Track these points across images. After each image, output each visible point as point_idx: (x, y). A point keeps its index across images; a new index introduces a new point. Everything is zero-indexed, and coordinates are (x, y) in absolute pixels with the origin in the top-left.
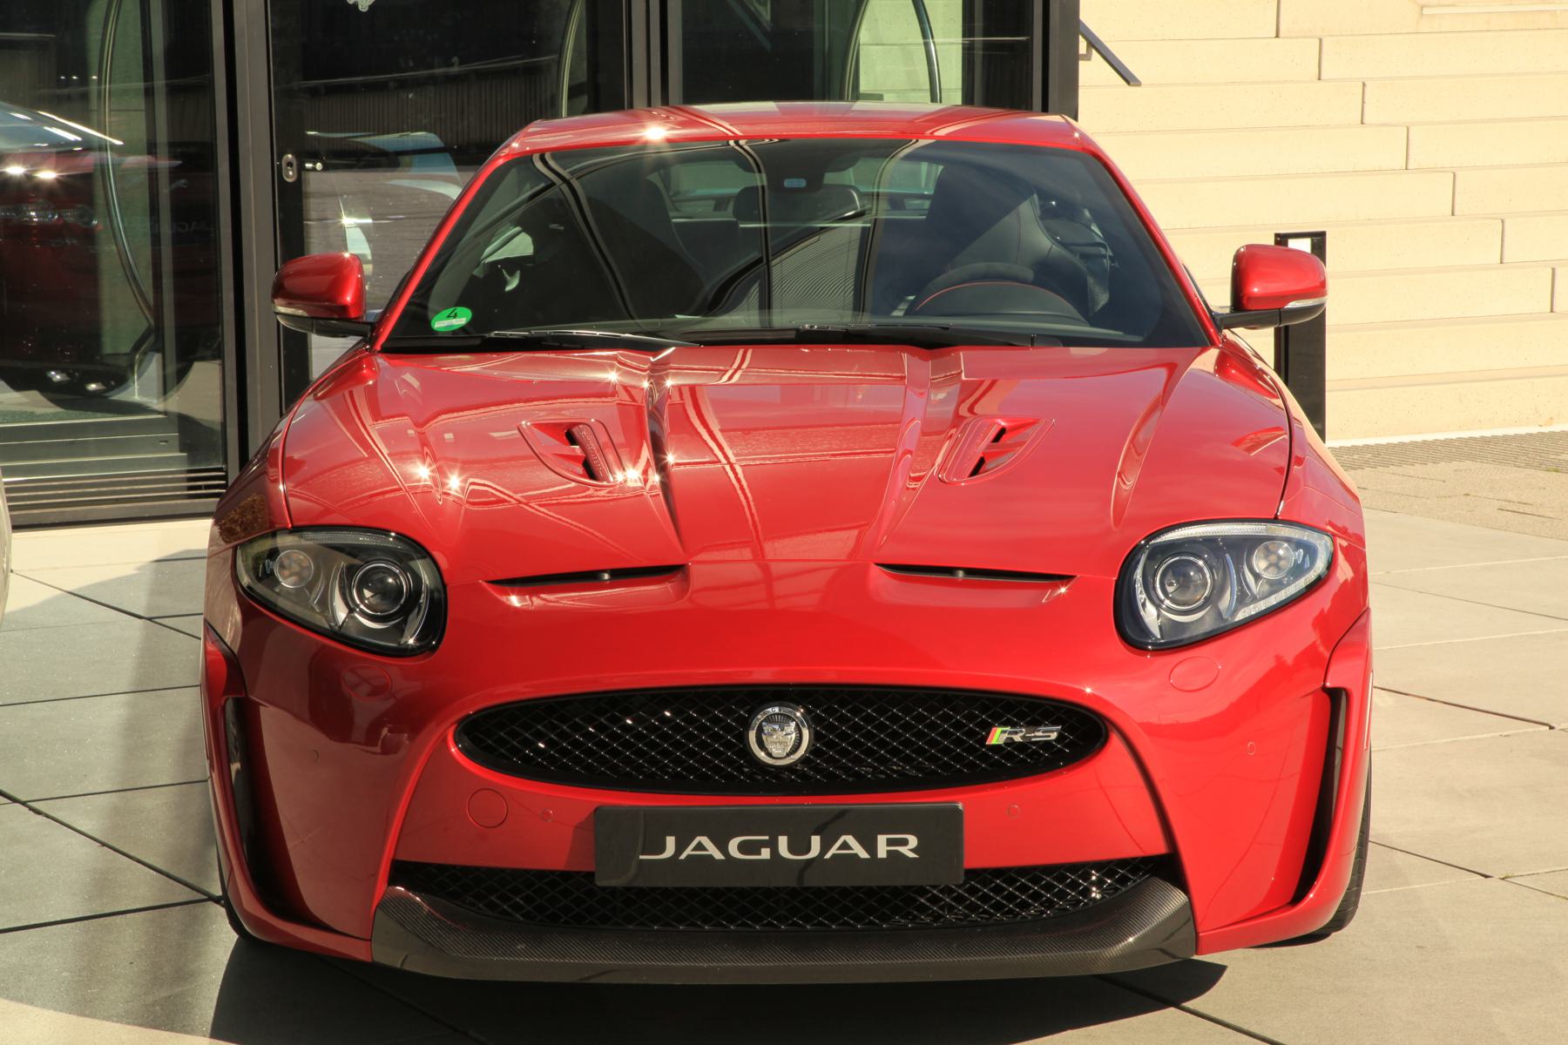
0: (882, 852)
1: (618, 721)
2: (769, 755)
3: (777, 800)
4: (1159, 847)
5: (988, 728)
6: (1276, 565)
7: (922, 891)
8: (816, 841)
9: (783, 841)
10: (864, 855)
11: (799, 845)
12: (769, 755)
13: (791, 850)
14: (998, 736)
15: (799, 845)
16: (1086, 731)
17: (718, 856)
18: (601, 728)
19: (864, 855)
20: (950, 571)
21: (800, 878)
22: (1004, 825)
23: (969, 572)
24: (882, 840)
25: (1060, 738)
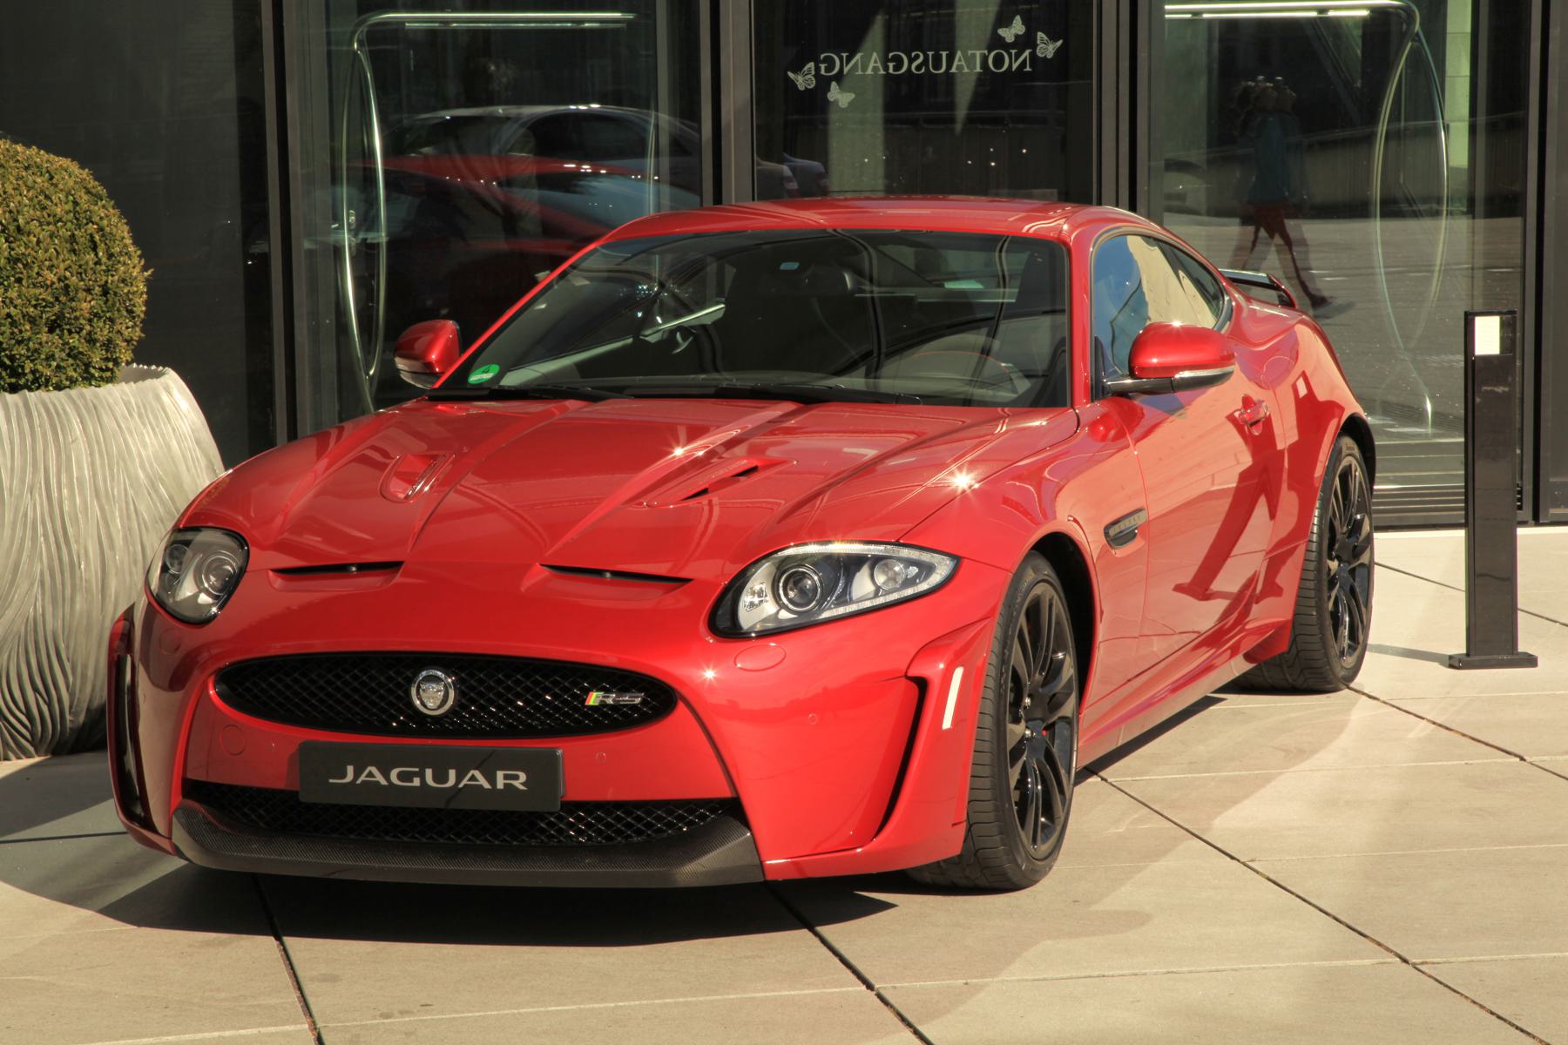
0: (500, 785)
1: (540, 697)
2: (423, 704)
3: (430, 741)
4: (726, 793)
5: (587, 691)
6: (894, 580)
7: (541, 816)
8: (452, 773)
9: (429, 773)
10: (487, 786)
11: (441, 777)
12: (423, 704)
13: (435, 779)
14: (594, 699)
15: (441, 777)
16: (661, 698)
17: (384, 782)
18: (499, 708)
19: (487, 786)
20: (600, 572)
21: (448, 802)
22: (594, 768)
23: (615, 573)
24: (500, 775)
25: (644, 702)
